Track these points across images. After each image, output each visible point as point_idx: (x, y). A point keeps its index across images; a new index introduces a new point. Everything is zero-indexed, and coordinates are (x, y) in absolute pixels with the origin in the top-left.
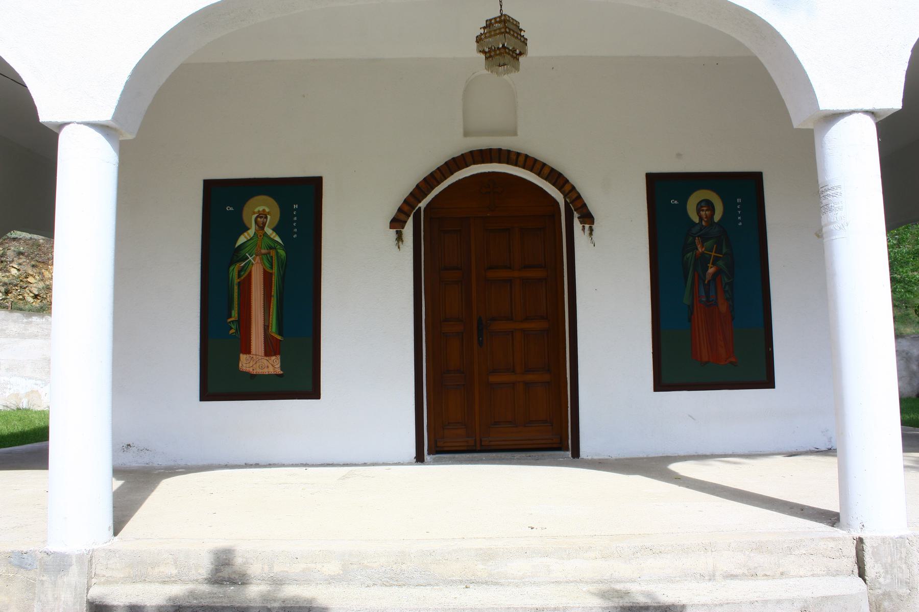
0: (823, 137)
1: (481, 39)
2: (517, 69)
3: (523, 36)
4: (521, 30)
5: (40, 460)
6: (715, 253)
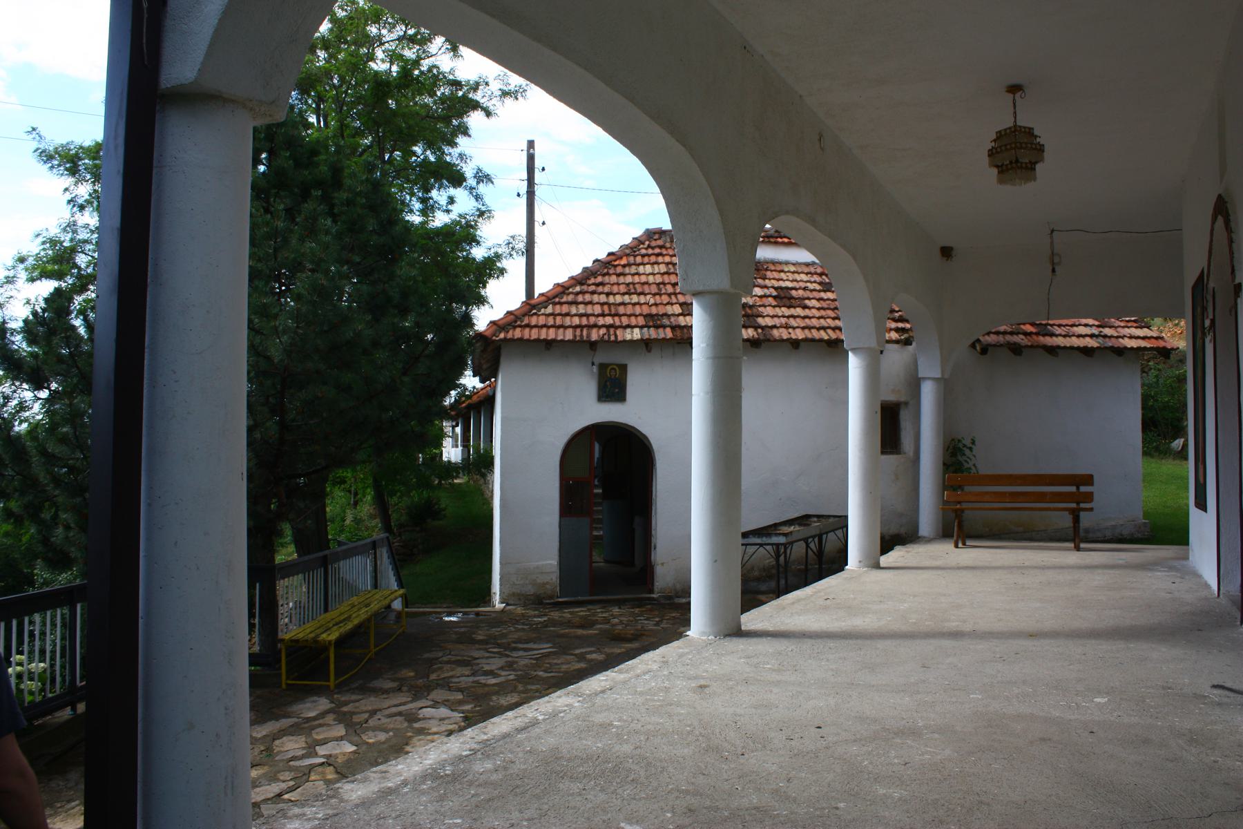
0: (900, 449)
2: (1035, 179)
4: (1036, 137)
6: (329, 681)
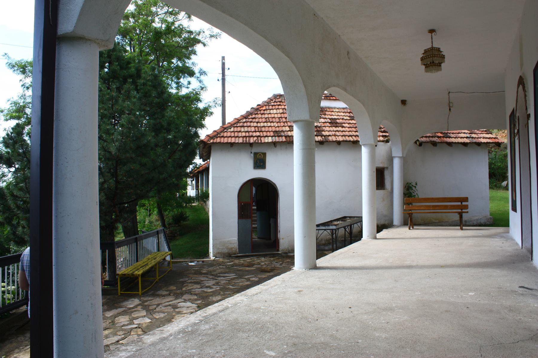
1: (423, 59)
3: (443, 54)
5: (224, 57)
